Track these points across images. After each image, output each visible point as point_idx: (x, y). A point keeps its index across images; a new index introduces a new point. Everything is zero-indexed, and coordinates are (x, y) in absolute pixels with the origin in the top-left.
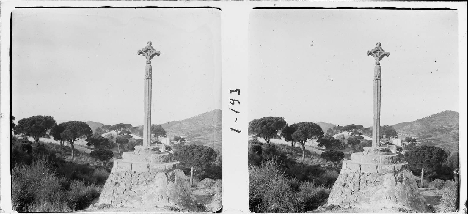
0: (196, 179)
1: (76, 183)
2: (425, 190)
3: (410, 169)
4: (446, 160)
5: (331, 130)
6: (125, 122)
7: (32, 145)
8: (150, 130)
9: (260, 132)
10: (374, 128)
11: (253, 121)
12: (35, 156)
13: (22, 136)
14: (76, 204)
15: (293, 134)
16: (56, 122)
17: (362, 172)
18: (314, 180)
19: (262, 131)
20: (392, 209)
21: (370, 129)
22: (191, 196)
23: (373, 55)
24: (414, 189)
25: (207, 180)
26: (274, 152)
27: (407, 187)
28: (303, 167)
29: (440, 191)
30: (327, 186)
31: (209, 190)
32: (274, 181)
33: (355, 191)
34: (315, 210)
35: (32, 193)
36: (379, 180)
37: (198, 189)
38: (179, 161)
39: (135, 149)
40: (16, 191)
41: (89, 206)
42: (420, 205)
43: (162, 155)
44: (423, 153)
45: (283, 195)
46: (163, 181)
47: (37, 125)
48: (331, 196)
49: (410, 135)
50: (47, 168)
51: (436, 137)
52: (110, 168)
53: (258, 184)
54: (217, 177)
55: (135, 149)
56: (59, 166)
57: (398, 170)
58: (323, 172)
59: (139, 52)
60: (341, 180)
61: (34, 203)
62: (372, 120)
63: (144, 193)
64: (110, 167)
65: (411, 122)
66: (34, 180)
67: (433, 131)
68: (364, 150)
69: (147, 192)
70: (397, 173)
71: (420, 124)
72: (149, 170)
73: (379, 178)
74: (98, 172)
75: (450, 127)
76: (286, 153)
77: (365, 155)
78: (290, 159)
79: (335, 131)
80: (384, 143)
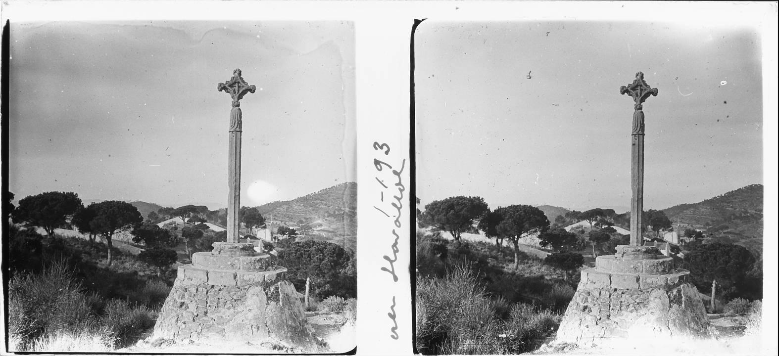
0: (315, 298)
1: (520, 309)
2: (718, 316)
3: (692, 282)
4: (753, 266)
5: (562, 218)
6: (197, 203)
7: (42, 240)
8: (239, 217)
9: (443, 223)
10: (633, 215)
11: (432, 204)
12: (47, 258)
13: (25, 226)
14: (115, 339)
15: (498, 225)
16: (488, 207)
17: (613, 287)
18: (534, 301)
19: (448, 219)
20: (260, 346)
21: (627, 216)
22: (306, 326)
23: (631, 94)
24: (298, 313)
25: (333, 300)
26: (467, 255)
27: (688, 312)
28: (516, 280)
29: (744, 318)
30: (556, 311)
31: (741, 317)
32: (467, 303)
33: (200, 315)
34: (536, 352)
35: (41, 320)
36: (642, 301)
37: (318, 314)
38: (287, 267)
39: (213, 248)
40: (15, 317)
41: (136, 342)
42: (308, 340)
43: (258, 258)
44: (714, 255)
45: (483, 326)
46: (260, 301)
47: (457, 212)
48: (159, 324)
49: (693, 225)
50: (66, 278)
51: (736, 229)
52: (171, 280)
53: (441, 308)
54: (349, 294)
55: (213, 248)
56: (88, 276)
57: (271, 281)
58: (144, 283)
59: (220, 88)
60: (578, 301)
61: (45, 338)
62: (630, 201)
63: (229, 321)
64: (172, 278)
65: (694, 204)
66: (448, 304)
67: (730, 218)
68: (616, 251)
69: (233, 320)
70: (270, 286)
71: (708, 207)
72: (237, 283)
73: (641, 297)
74: (151, 286)
75: (759, 213)
76: (487, 257)
77: (214, 256)
78: (493, 266)
79: (568, 220)
80: (650, 240)
